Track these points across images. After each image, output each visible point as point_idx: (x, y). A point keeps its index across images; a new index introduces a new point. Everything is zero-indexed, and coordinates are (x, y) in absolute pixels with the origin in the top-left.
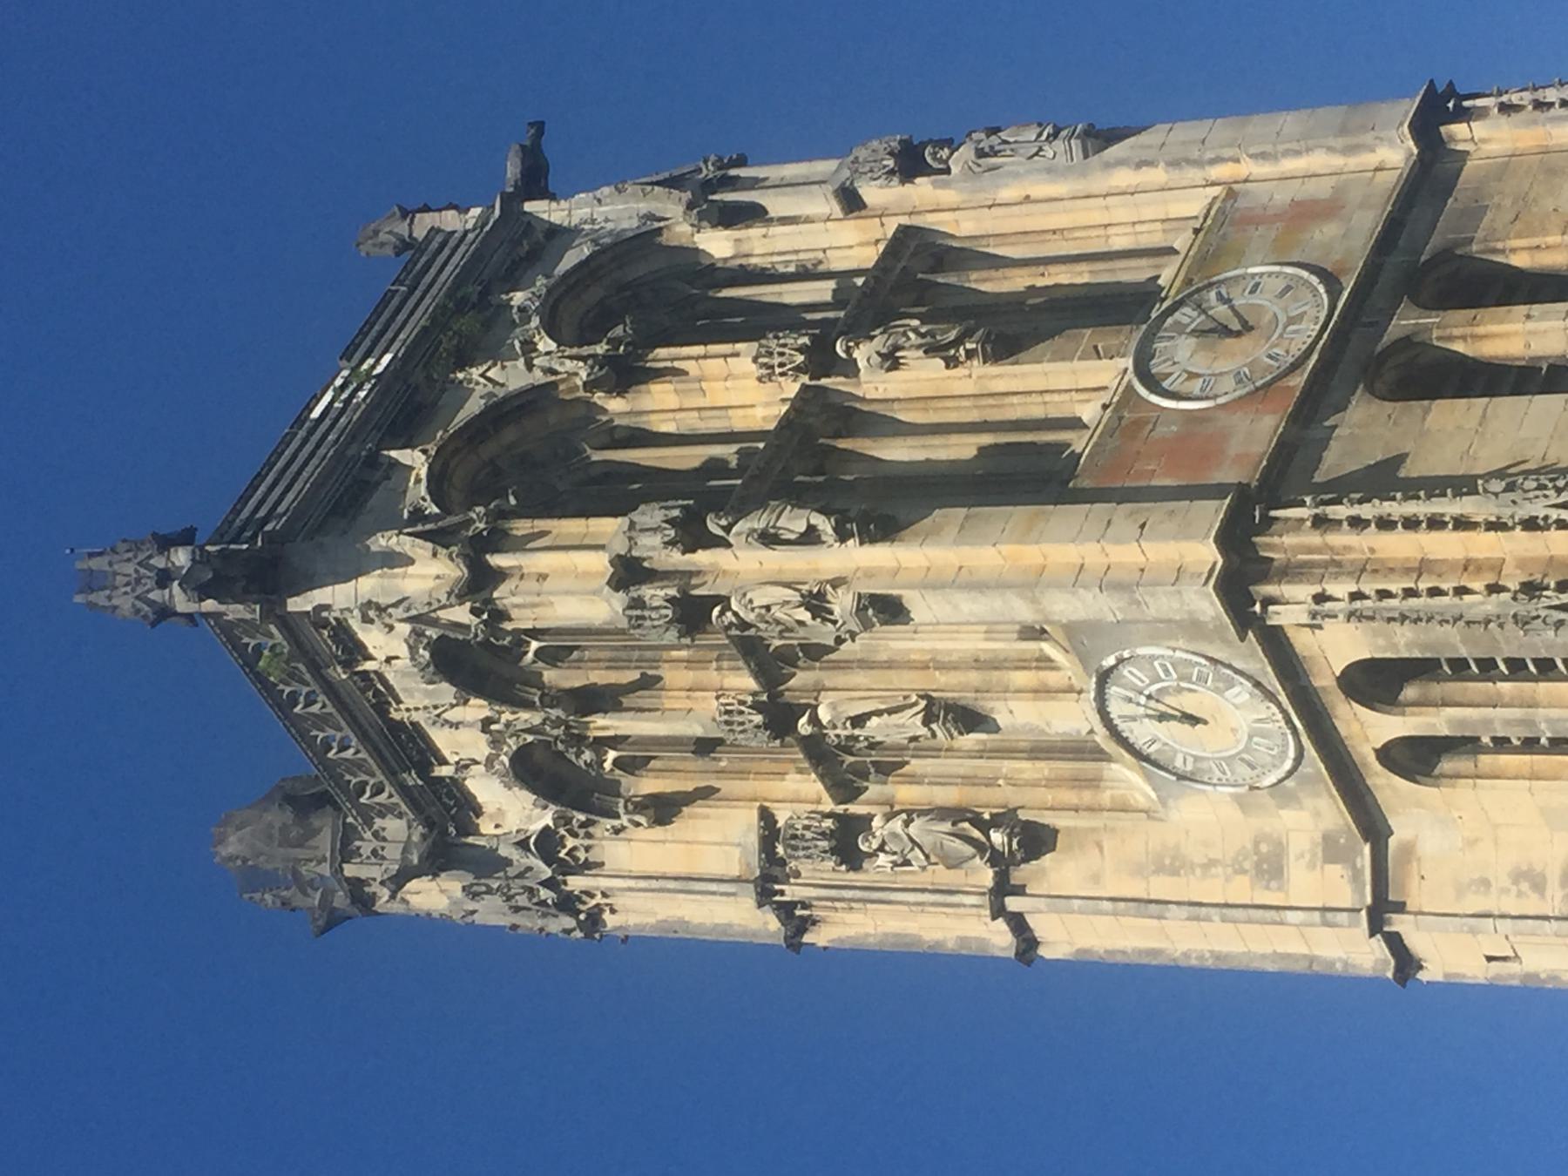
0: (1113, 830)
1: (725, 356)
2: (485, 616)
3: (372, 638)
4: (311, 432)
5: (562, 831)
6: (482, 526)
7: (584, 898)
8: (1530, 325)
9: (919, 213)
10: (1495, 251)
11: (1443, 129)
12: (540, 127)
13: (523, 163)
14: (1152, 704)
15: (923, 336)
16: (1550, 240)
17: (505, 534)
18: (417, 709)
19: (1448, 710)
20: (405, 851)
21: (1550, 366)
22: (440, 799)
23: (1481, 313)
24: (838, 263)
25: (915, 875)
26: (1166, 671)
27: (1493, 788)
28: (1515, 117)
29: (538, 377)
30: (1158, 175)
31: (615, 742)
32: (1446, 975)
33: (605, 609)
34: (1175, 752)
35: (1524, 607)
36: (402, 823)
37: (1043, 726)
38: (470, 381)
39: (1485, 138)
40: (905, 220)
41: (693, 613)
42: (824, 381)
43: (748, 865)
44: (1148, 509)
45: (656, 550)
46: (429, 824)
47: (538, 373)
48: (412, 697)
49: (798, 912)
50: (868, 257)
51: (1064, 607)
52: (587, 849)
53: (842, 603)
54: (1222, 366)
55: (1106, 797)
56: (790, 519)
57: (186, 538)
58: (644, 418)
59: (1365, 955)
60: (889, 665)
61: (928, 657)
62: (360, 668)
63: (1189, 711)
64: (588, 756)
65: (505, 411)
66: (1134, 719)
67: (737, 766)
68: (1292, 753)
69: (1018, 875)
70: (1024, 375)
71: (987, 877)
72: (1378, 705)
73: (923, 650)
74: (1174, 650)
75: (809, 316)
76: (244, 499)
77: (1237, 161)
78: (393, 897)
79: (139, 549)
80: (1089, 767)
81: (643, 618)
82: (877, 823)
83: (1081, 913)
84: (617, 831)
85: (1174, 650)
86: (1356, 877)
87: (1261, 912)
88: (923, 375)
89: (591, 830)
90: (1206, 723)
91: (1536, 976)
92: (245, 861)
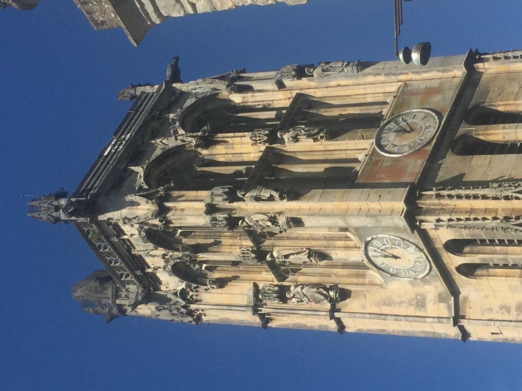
0: (369, 291)
1: (241, 137)
2: (164, 222)
3: (126, 228)
4: (104, 160)
5: (188, 290)
6: (163, 193)
7: (196, 311)
8: (505, 131)
9: (303, 89)
10: (493, 105)
11: (475, 65)
12: (177, 59)
13: (172, 70)
14: (383, 252)
15: (306, 131)
16: (511, 102)
17: (170, 195)
18: (141, 251)
19: (480, 255)
20: (137, 296)
21: (511, 144)
22: (148, 279)
23: (488, 126)
24: (277, 105)
25: (305, 305)
26: (387, 242)
27: (493, 279)
28: (499, 61)
29: (179, 143)
30: (382, 78)
31: (205, 262)
32: (478, 339)
33: (204, 220)
34: (390, 267)
35: (504, 225)
36: (135, 286)
37: (347, 258)
38: (156, 144)
39: (488, 68)
40: (299, 92)
41: (233, 222)
42: (273, 145)
43: (250, 301)
44: (381, 191)
45: (220, 202)
46: (144, 287)
47: (179, 142)
48: (139, 247)
49: (266, 317)
50: (287, 103)
51: (355, 222)
52: (197, 295)
53: (282, 220)
54: (404, 143)
55: (367, 280)
56: (264, 193)
57: (64, 195)
58: (214, 157)
59: (451, 332)
60: (297, 238)
61: (309, 236)
62: (122, 238)
63: (395, 254)
64: (197, 266)
65: (168, 154)
66: (377, 257)
67: (245, 269)
68: (428, 268)
69: (339, 305)
70: (340, 144)
71: (328, 306)
72: (458, 254)
73: (307, 234)
74: (390, 235)
75: (268, 123)
76: (83, 182)
77: (408, 74)
78: (132, 310)
79: (49, 199)
80: (361, 271)
81: (216, 224)
82: (292, 288)
83: (360, 318)
84: (206, 290)
85: (390, 235)
86: (449, 308)
87: (418, 318)
88: (306, 144)
89: (198, 289)
90: (400, 258)
91: (507, 339)
92: (83, 297)
